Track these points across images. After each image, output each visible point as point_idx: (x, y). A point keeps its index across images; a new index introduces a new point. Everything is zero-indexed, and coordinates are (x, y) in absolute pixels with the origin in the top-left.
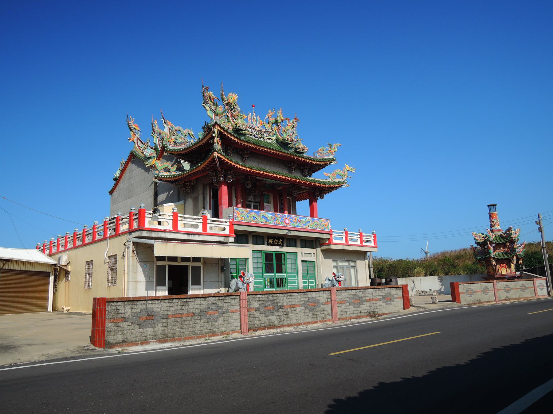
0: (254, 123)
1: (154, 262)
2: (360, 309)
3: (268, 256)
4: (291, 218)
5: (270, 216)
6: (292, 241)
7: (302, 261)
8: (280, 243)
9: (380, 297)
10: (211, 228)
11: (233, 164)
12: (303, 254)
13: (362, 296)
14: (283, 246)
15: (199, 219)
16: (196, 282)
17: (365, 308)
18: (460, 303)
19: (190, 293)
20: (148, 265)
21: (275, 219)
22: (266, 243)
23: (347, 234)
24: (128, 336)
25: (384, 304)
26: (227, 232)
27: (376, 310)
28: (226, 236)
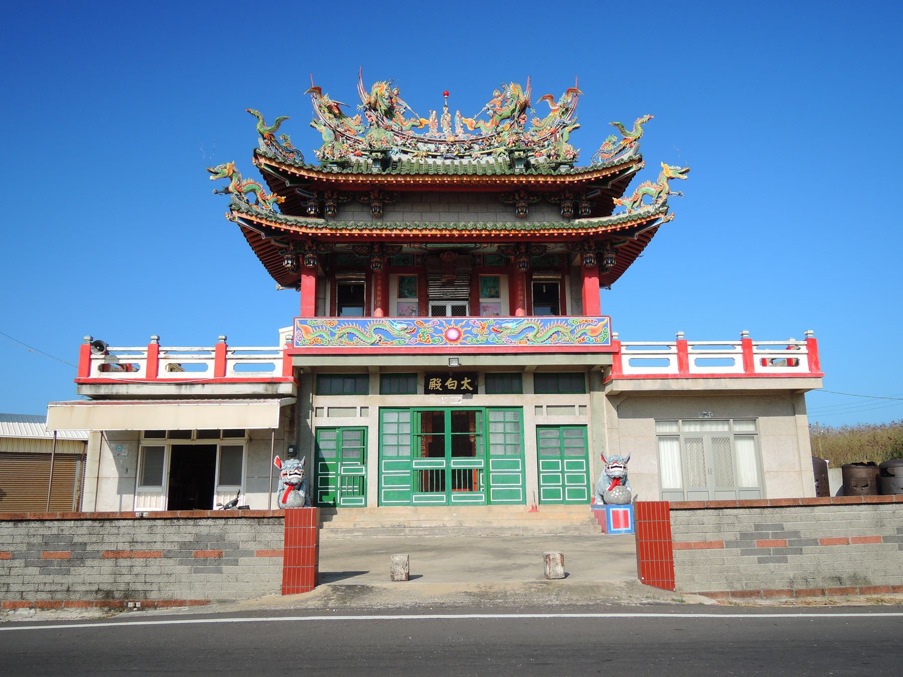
0: (446, 130)
1: (139, 441)
2: (68, 580)
3: (431, 419)
4: (467, 325)
5: (399, 326)
6: (505, 379)
7: (538, 426)
9: (169, 547)
10: (236, 368)
12: (536, 408)
13: (85, 539)
14: (475, 392)
15: (208, 352)
16: (232, 478)
17: (89, 579)
18: (668, 583)
19: (221, 499)
20: (127, 445)
22: (421, 388)
23: (682, 347)
25: (184, 569)
26: (278, 373)
27: (139, 587)
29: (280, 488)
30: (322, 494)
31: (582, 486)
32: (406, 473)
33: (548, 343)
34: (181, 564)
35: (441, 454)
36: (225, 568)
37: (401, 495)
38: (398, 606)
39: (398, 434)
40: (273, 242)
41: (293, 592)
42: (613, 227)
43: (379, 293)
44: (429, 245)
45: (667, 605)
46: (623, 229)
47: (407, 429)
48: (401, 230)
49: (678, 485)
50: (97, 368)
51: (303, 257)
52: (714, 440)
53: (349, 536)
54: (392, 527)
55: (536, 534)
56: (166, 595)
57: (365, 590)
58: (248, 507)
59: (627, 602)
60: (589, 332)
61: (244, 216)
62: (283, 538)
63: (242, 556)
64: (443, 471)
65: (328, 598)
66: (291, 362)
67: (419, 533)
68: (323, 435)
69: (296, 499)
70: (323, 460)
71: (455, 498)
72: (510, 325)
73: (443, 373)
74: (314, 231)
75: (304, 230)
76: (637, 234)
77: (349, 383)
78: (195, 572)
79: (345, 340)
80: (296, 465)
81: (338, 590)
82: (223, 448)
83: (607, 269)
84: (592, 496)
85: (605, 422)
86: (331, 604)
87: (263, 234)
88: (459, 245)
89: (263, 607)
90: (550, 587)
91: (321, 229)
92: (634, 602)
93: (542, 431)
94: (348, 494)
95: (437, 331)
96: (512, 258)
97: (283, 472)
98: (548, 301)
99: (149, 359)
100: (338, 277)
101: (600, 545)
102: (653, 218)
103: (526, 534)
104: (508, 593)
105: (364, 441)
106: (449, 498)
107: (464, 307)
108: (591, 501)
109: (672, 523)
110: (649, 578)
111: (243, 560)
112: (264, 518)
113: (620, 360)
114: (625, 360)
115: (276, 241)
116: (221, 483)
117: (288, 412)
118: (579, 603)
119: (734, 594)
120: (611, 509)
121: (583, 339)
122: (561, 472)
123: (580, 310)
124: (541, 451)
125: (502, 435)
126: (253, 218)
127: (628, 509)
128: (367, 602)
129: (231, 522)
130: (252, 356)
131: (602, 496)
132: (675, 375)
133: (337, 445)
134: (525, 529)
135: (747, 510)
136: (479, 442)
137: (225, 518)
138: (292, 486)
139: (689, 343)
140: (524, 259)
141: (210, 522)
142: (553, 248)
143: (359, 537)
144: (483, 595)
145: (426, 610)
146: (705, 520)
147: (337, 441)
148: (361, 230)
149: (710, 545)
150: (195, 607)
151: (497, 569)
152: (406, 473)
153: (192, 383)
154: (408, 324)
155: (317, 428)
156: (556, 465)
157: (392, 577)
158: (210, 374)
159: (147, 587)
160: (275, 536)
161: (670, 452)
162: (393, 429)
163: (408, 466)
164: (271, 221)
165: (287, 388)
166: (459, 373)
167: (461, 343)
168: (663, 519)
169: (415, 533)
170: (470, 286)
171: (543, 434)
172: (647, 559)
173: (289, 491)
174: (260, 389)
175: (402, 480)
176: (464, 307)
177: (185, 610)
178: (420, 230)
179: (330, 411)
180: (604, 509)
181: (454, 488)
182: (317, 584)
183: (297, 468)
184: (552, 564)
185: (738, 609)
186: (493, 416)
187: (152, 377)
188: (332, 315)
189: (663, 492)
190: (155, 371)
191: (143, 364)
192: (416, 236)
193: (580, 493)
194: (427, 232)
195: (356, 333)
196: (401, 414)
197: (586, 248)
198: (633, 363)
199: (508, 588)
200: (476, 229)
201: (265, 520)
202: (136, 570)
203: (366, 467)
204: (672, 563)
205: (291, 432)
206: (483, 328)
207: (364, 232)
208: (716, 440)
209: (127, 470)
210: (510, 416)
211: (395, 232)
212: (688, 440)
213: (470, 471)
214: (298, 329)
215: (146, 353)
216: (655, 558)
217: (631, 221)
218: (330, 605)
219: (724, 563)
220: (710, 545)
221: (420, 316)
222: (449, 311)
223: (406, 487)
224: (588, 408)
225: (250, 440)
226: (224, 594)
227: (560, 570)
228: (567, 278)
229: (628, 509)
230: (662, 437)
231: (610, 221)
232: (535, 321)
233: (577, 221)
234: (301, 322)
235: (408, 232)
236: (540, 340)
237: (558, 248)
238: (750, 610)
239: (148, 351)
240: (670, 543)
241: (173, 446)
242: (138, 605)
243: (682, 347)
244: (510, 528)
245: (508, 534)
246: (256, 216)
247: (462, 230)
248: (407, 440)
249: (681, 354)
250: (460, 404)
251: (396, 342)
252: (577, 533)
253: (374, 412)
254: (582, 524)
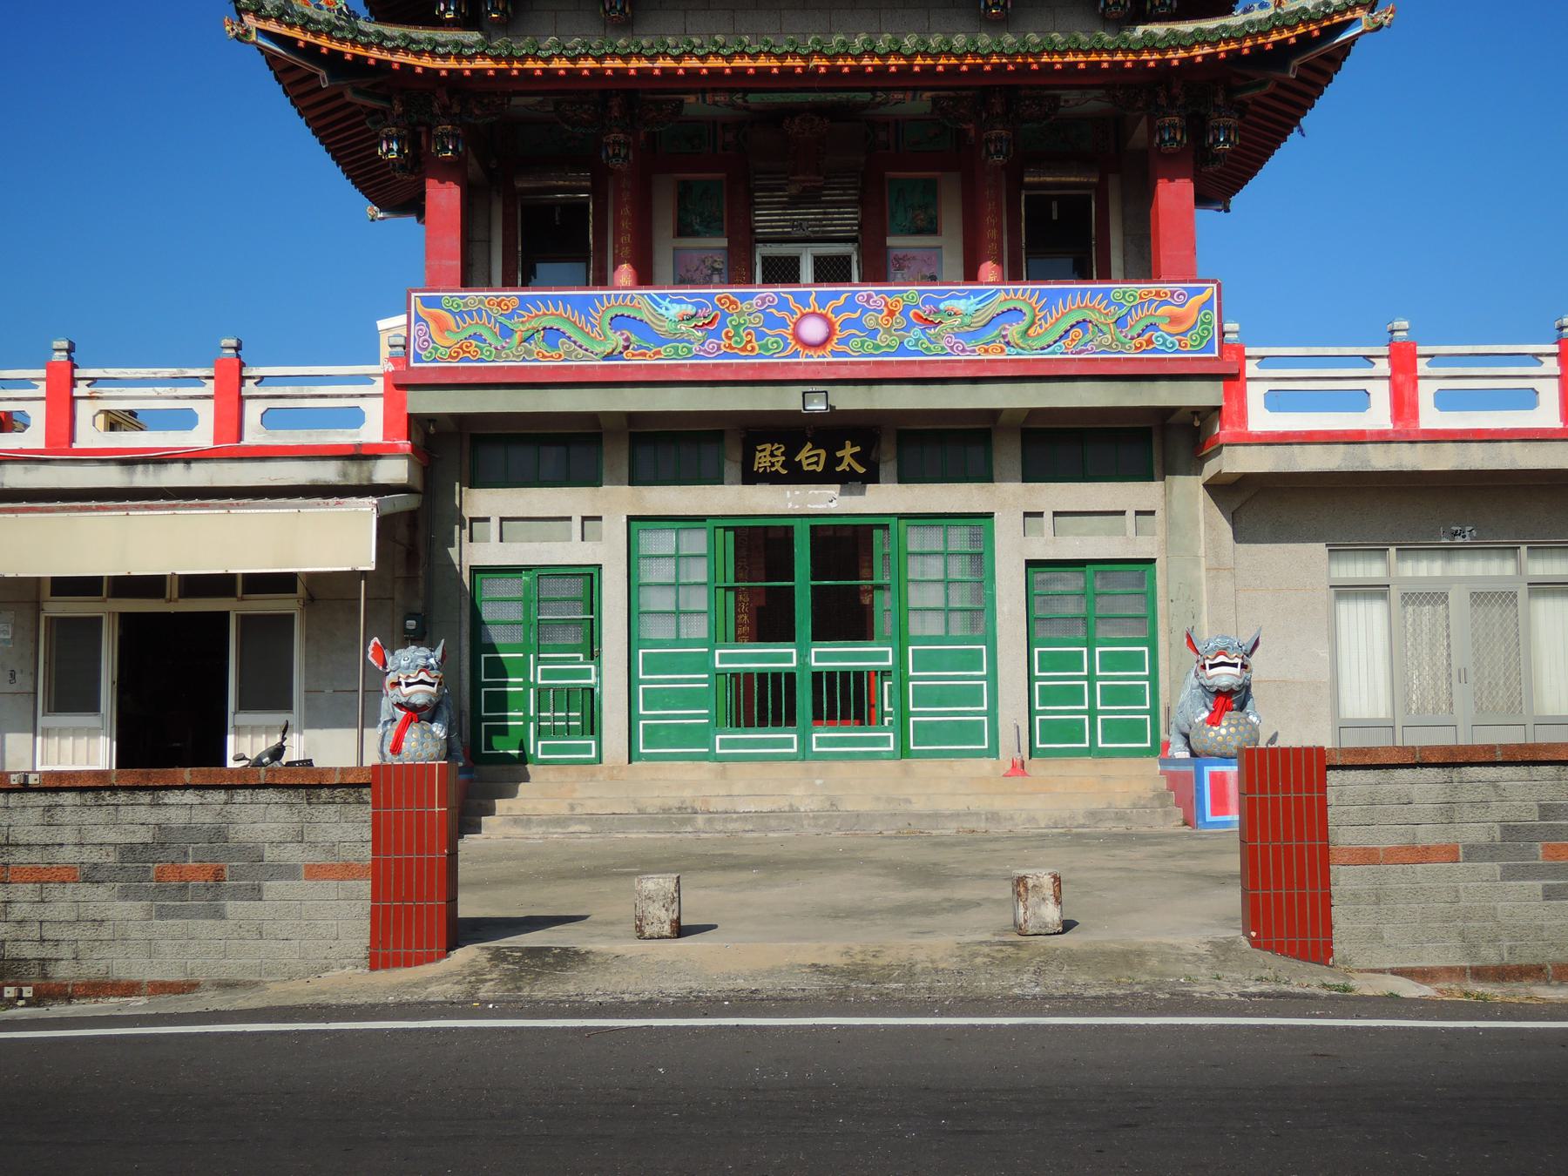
1: (37, 606)
3: (760, 547)
4: (851, 305)
5: (675, 310)
6: (949, 445)
7: (1030, 564)
9: (93, 856)
10: (267, 419)
11: (374, 53)
12: (1026, 519)
14: (872, 477)
16: (270, 695)
18: (1318, 950)
19: (244, 744)
21: (711, 325)
22: (732, 469)
23: (1403, 361)
26: (372, 432)
27: (29, 951)
28: (362, 455)
29: (384, 717)
30: (491, 731)
31: (1138, 712)
32: (699, 681)
34: (126, 897)
35: (785, 633)
36: (230, 906)
37: (685, 735)
38: (646, 996)
39: (676, 585)
40: (349, 96)
41: (397, 965)
42: (1233, 46)
43: (625, 224)
44: (753, 98)
45: (1305, 996)
46: (1258, 50)
47: (699, 572)
48: (677, 58)
49: (1382, 711)
51: (429, 132)
52: (1478, 598)
53: (556, 834)
54: (665, 811)
55: (1019, 829)
56: (92, 969)
57: (568, 958)
58: (308, 763)
59: (1207, 989)
60: (1164, 325)
61: (272, 26)
62: (368, 835)
63: (271, 878)
64: (791, 677)
65: (478, 977)
66: (404, 403)
67: (731, 826)
68: (492, 588)
69: (423, 744)
70: (492, 648)
71: (820, 742)
72: (961, 305)
73: (788, 431)
74: (452, 64)
75: (426, 62)
76: (1295, 63)
77: (552, 454)
78: (160, 916)
79: (538, 345)
80: (421, 662)
81: (504, 959)
82: (244, 620)
83: (1216, 157)
84: (1163, 736)
85: (1202, 552)
86: (485, 991)
87: (322, 73)
88: (830, 97)
89: (321, 999)
90: (1024, 954)
91: (471, 58)
92: (1228, 989)
93: (1040, 576)
94: (555, 732)
95: (771, 322)
96: (971, 128)
97: (392, 678)
98: (1065, 239)
99: (49, 399)
100: (521, 184)
101: (1171, 856)
102: (1337, 19)
103: (994, 830)
104: (919, 967)
105: (592, 601)
106: (805, 742)
107: (847, 259)
108: (1159, 749)
109: (1331, 797)
110: (1268, 934)
111: (273, 887)
112: (321, 786)
113: (1242, 395)
114: (1255, 394)
115: (357, 91)
116: (243, 706)
117: (402, 532)
118: (1092, 993)
119: (1479, 974)
120: (1207, 770)
121: (1149, 342)
122: (1086, 678)
123: (1144, 267)
124: (1036, 626)
125: (940, 588)
126: (296, 33)
128: (571, 988)
129: (240, 796)
130: (306, 390)
131: (1187, 737)
133: (527, 612)
134: (993, 817)
135: (1522, 771)
136: (882, 604)
137: (227, 788)
138: (415, 713)
139: (1421, 350)
140: (999, 131)
141: (190, 797)
142: (1076, 102)
143: (582, 836)
144: (854, 972)
145: (712, 1006)
146: (1416, 792)
147: (525, 601)
148: (573, 59)
149: (1422, 854)
150: (163, 998)
151: (903, 910)
152: (699, 681)
153: (161, 459)
154: (699, 305)
155: (475, 570)
156: (1073, 662)
157: (639, 929)
158: (202, 436)
159: (47, 952)
160: (348, 830)
161: (1364, 625)
162: (661, 572)
163: (703, 663)
164: (342, 40)
165: (393, 471)
166: (831, 431)
167: (834, 353)
168: (1310, 790)
169: (719, 827)
170: (861, 202)
171: (1044, 582)
172: (1266, 886)
173: (406, 724)
174: (328, 472)
175: (689, 698)
176: (847, 259)
177: (138, 1004)
178: (728, 58)
179: (509, 529)
180: (1191, 769)
181: (817, 717)
182: (453, 944)
183: (426, 668)
184: (1032, 899)
185: (1484, 1009)
186: (917, 539)
187: (61, 446)
188: (509, 282)
189: (1342, 727)
190: (66, 430)
191: (37, 414)
192: (715, 73)
193: (1132, 730)
194: (745, 62)
195: (565, 327)
196: (684, 535)
197: (1162, 101)
198: (1276, 401)
199: (920, 956)
200: (872, 54)
201: (325, 793)
202: (18, 911)
203: (599, 666)
204: (1328, 897)
205: (410, 580)
206: (891, 313)
207: (582, 64)
208: (1481, 598)
209: (13, 675)
210: (959, 538)
211: (660, 63)
212: (1409, 598)
213: (859, 675)
214: (419, 319)
215: (43, 386)
216: (1286, 882)
217: (1279, 30)
218: (482, 994)
219: (1457, 900)
220: (1422, 854)
221: (732, 281)
222: (807, 271)
223: (699, 716)
224: (1161, 522)
225: (311, 600)
226: (231, 968)
227: (1051, 914)
228: (1113, 182)
230: (1346, 591)
231: (1225, 28)
232: (1025, 294)
233: (1140, 30)
234: (426, 302)
235: (694, 63)
236: (1037, 344)
237: (1092, 103)
238: (1510, 1012)
239: (47, 379)
240: (1325, 850)
241: (122, 615)
242: (28, 992)
243: (1403, 361)
244: (956, 816)
245: (950, 829)
246: (304, 28)
247: (837, 56)
248: (699, 600)
249: (1400, 378)
250: (834, 508)
251: (666, 350)
252: (1121, 828)
253: (615, 529)
254: (1134, 806)
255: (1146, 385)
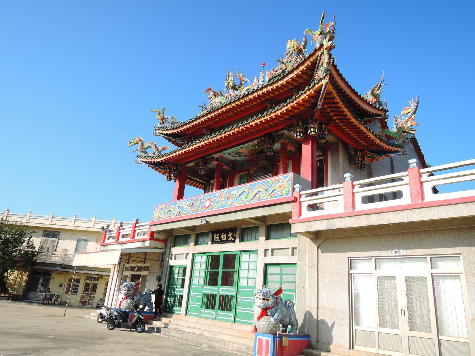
3: (214, 260)
8: (231, 238)
24: (216, 344)
33: (252, 202)
50: (404, 194)
85: (307, 261)
127: (270, 339)
132: (409, 205)
167: (211, 209)
229: (270, 339)
255: (273, 207)
